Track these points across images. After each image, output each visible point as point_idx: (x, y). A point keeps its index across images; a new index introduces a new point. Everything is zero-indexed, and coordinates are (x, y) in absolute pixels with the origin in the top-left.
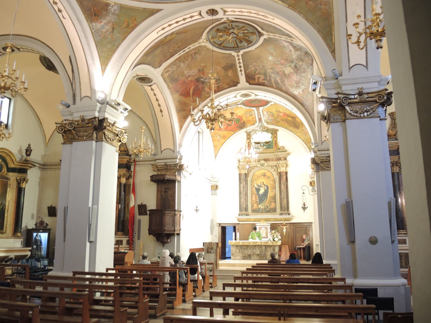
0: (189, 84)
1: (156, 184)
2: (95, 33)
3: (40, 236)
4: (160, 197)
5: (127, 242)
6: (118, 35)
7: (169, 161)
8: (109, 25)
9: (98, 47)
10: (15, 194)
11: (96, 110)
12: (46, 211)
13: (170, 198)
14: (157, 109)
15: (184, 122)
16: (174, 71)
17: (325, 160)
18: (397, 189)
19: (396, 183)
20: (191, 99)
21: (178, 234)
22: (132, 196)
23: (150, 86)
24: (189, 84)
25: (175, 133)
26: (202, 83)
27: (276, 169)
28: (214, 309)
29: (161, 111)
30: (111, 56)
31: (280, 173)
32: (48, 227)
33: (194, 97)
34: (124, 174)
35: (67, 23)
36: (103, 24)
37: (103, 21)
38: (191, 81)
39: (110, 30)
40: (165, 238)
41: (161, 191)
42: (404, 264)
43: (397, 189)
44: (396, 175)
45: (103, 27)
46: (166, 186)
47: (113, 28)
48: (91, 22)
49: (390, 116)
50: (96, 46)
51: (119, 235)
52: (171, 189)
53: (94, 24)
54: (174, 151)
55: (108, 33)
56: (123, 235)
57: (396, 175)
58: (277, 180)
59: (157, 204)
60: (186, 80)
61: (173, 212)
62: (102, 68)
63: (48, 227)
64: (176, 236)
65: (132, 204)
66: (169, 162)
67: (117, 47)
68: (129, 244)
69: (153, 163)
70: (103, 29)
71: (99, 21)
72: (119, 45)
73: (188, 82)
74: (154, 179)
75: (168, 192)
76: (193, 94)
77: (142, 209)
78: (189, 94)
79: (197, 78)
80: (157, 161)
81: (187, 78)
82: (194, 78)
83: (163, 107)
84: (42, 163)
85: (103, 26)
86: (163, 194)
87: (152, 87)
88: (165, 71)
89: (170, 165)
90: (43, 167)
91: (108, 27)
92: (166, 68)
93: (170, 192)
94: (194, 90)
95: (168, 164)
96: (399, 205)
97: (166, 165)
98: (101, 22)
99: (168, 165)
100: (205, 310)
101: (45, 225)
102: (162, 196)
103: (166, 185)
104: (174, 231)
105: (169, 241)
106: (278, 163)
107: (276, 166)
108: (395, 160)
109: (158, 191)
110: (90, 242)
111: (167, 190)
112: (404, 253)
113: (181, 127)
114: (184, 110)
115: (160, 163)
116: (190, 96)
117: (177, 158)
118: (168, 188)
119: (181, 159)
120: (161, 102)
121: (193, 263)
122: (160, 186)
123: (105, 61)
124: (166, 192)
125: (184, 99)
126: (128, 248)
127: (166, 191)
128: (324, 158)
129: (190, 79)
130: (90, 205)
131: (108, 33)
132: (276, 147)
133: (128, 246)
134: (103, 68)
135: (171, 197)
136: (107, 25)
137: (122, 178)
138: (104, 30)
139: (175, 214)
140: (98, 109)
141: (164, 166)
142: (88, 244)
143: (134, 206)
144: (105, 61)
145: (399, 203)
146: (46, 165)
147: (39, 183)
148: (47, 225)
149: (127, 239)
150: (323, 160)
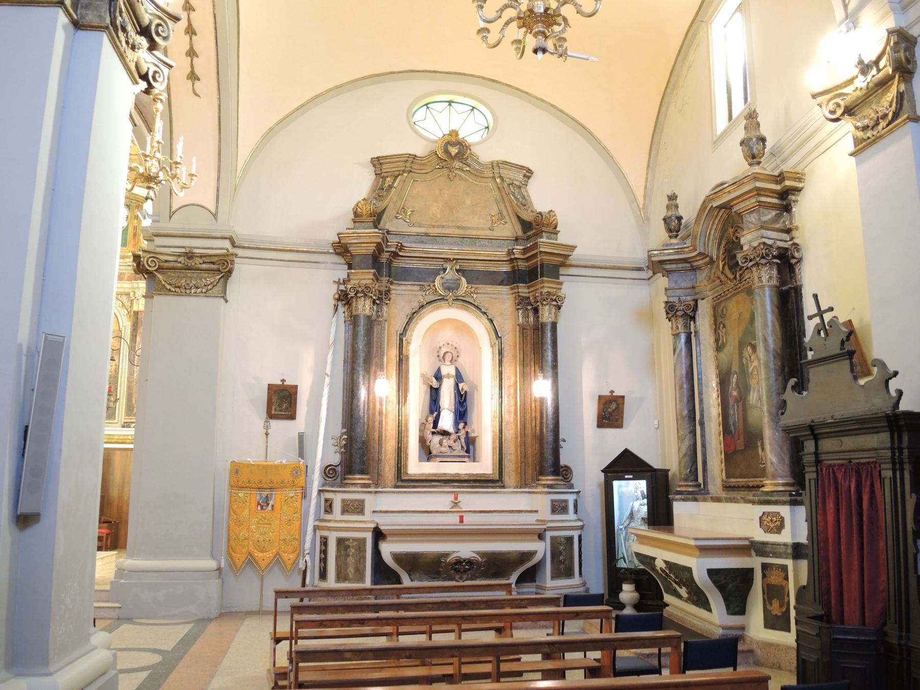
10: (69, 399)
17: (172, 264)
18: (361, 360)
19: (361, 345)
27: (127, 304)
31: (136, 313)
42: (351, 570)
43: (361, 360)
44: (362, 322)
49: (374, 166)
57: (362, 322)
58: (127, 334)
96: (357, 406)
100: (620, 497)
106: (135, 285)
107: (128, 294)
108: (364, 282)
112: (355, 540)
128: (170, 258)
132: (135, 245)
145: (358, 400)
150: (166, 265)
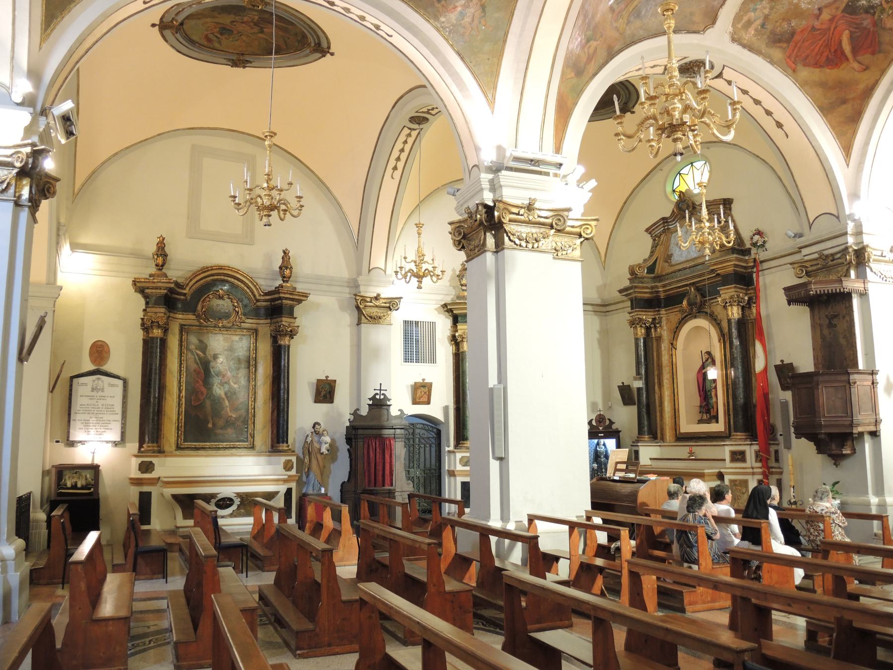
0: (829, 29)
1: (807, 309)
2: (451, 34)
3: (604, 445)
4: (820, 340)
5: (757, 456)
6: (496, 15)
7: (829, 244)
8: (471, 4)
9: (467, 60)
11: (482, 190)
12: (617, 395)
13: (843, 341)
14: (768, 124)
15: (854, 133)
16: (766, 17)
20: (856, 65)
21: (875, 434)
22: (758, 347)
23: (720, 76)
24: (829, 29)
25: (831, 168)
26: (867, 12)
28: (878, 648)
29: (779, 125)
30: (499, 65)
32: (614, 427)
33: (859, 58)
34: (731, 297)
35: (397, 40)
36: (459, 9)
37: (457, 4)
38: (831, 20)
39: (478, 13)
40: (834, 446)
41: (821, 325)
45: (462, 15)
46: (830, 311)
47: (483, 7)
48: (436, 18)
50: (462, 59)
51: (736, 440)
52: (844, 317)
53: (443, 19)
54: (838, 217)
55: (476, 21)
56: (745, 440)
59: (816, 358)
60: (817, 24)
61: (845, 378)
62: (486, 96)
63: (614, 427)
64: (867, 437)
65: (759, 365)
66: (830, 247)
67: (505, 41)
68: (761, 461)
69: (797, 257)
70: (463, 19)
71: (451, 7)
72: (506, 35)
73: (824, 27)
74: (795, 296)
75: (835, 326)
76: (855, 51)
77: (786, 372)
78: (843, 53)
79: (847, 5)
80: (805, 251)
81: (818, 17)
82: (837, 8)
83: (780, 114)
84: (599, 302)
85: (461, 13)
86: (826, 332)
87: (725, 76)
88: (739, 26)
89: (832, 255)
90: (604, 309)
91: (472, 10)
92: (737, 18)
93: (841, 326)
94: (851, 37)
95: (826, 253)
97: (823, 257)
98: (455, 7)
99: (827, 256)
101: (607, 422)
102: (823, 337)
103: (830, 309)
104: (851, 425)
105: (847, 451)
109: (813, 327)
110: (501, 459)
111: (835, 321)
113: (847, 149)
114: (844, 102)
115: (811, 253)
116: (847, 59)
117: (846, 234)
118: (836, 316)
119: (859, 233)
120: (769, 102)
121: (755, 514)
122: (816, 311)
123: (488, 80)
124: (831, 326)
125: (831, 74)
126: (760, 470)
127: (830, 323)
129: (826, 16)
130: (493, 381)
131: (476, 21)
133: (759, 465)
134: (490, 96)
135: (845, 337)
136: (468, 7)
137: (729, 308)
138: (467, 20)
139: (849, 383)
140: (486, 185)
141: (820, 262)
142: (494, 465)
143: (766, 369)
144: (488, 80)
146: (607, 305)
147: (600, 342)
148: (611, 423)
149: (756, 447)
